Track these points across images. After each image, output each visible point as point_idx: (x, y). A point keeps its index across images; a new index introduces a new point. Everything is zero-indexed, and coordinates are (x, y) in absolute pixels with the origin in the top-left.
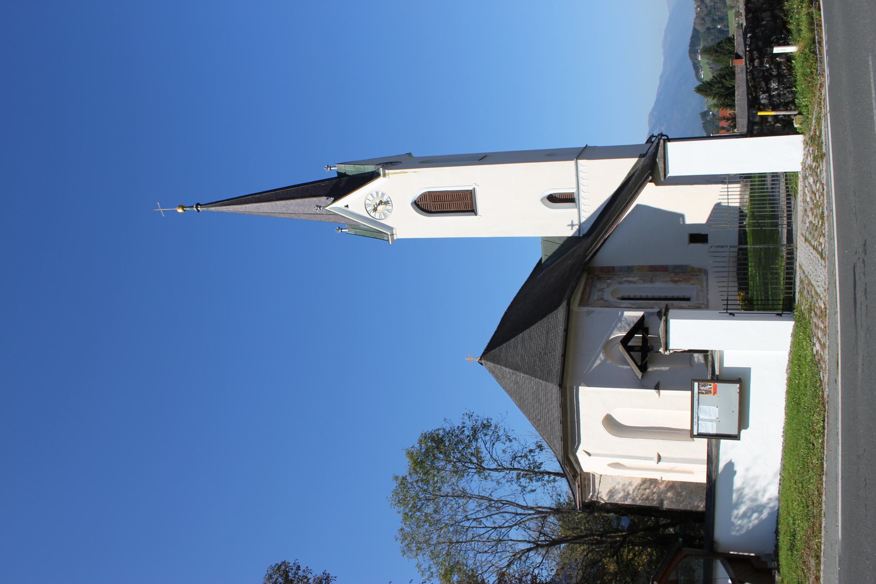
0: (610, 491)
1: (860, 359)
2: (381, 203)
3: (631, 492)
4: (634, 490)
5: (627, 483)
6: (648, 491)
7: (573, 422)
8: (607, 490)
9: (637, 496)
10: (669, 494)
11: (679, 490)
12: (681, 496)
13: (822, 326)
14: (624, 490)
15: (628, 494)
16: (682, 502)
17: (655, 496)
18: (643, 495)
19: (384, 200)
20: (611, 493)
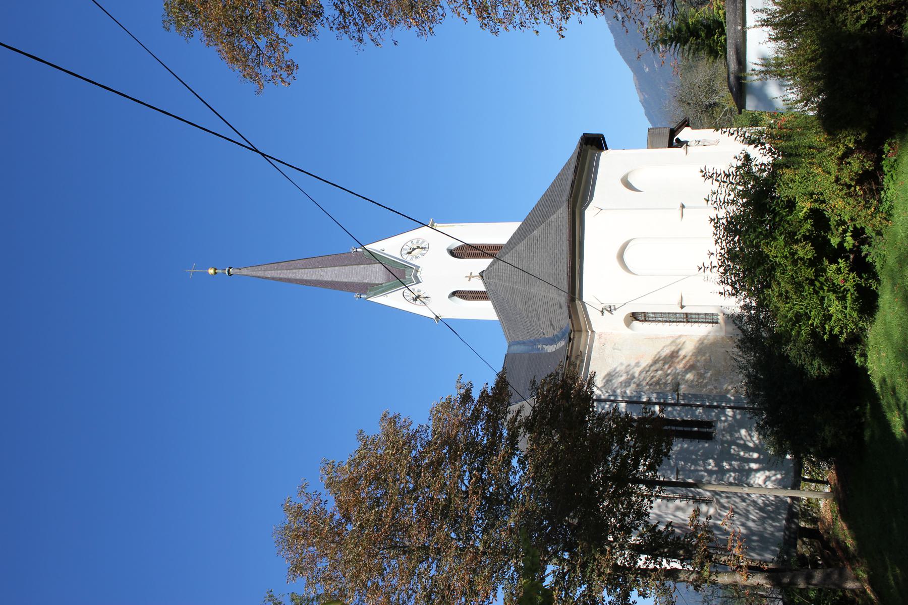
0: (609, 375)
1: (740, 578)
2: (418, 247)
3: (636, 375)
4: (641, 372)
5: (633, 364)
6: (660, 372)
7: (588, 182)
8: (606, 373)
9: (644, 379)
10: (689, 376)
11: (702, 371)
12: (704, 378)
13: (706, 574)
14: (627, 373)
15: (634, 377)
16: (706, 385)
17: (670, 378)
18: (652, 377)
19: (423, 246)
20: (609, 378)
